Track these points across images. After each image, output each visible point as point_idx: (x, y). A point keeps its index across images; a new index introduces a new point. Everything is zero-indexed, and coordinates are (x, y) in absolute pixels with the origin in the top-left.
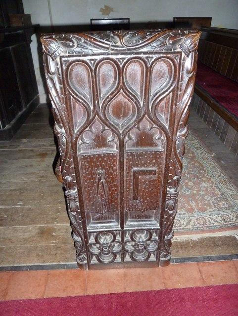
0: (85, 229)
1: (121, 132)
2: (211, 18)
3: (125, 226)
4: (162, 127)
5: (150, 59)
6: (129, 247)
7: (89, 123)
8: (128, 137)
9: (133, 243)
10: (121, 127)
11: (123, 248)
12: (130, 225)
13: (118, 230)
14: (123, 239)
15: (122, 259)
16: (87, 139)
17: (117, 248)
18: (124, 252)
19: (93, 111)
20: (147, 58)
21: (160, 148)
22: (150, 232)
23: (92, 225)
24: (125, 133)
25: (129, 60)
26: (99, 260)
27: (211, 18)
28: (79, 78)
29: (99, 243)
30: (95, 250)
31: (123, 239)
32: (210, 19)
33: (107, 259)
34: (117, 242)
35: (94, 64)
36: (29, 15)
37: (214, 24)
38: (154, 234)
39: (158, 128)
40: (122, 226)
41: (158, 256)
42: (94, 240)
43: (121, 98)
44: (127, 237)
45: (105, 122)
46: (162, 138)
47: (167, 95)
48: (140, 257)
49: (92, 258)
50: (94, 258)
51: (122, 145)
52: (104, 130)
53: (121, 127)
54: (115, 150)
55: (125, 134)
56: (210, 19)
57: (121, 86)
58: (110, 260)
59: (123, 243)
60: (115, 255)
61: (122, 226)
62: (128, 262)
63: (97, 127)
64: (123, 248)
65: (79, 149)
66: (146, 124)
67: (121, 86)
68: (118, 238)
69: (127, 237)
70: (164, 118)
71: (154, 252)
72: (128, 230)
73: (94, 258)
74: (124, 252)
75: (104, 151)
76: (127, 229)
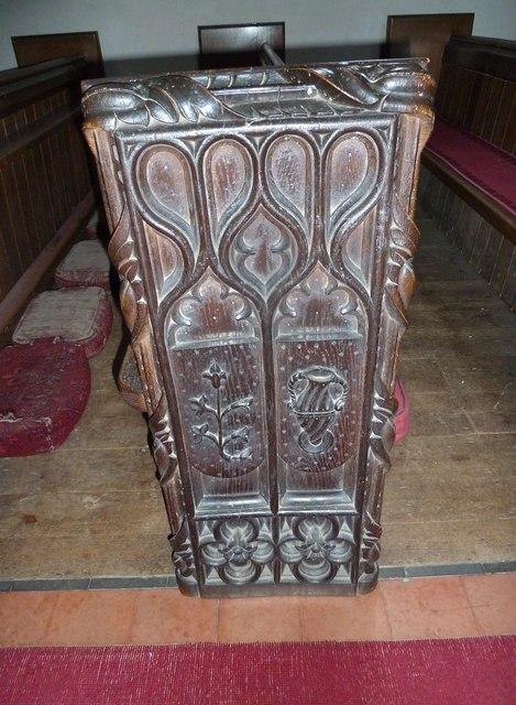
0: (189, 509)
1: (266, 299)
2: (473, 15)
3: (280, 507)
4: (355, 288)
5: (322, 136)
6: (291, 552)
7: (188, 282)
8: (281, 310)
9: (300, 543)
10: (164, 287)
11: (277, 552)
12: (289, 501)
13: (264, 516)
14: (276, 536)
15: (352, 579)
16: (186, 311)
17: (263, 554)
18: (277, 563)
19: (200, 259)
20: (313, 132)
21: (354, 331)
22: (333, 522)
23: (205, 504)
24: (275, 300)
25: (279, 135)
26: (297, 575)
27: (473, 15)
28: (163, 177)
29: (303, 539)
30: (215, 557)
31: (276, 536)
32: (468, 19)
33: (240, 575)
34: (263, 541)
35: (261, 145)
36: (95, 33)
37: (480, 30)
38: (265, 526)
39: (347, 290)
40: (274, 507)
41: (355, 577)
42: (291, 532)
43: (260, 220)
44: (286, 530)
45: (230, 281)
46: (253, 315)
47: (365, 214)
48: (240, 575)
49: (201, 530)
50: (214, 573)
51: (267, 330)
52: (227, 294)
53: (265, 289)
54: (253, 336)
55: (275, 300)
56: (468, 19)
57: (260, 203)
58: (325, 575)
59: (276, 546)
60: (258, 568)
61: (274, 507)
62: (288, 584)
63: (209, 286)
64: (277, 552)
65: (172, 342)
66: (321, 282)
67: (260, 203)
68: (265, 531)
69: (286, 530)
70: (356, 265)
71: (346, 565)
72: (284, 515)
73: (214, 573)
74: (277, 563)
75: (229, 338)
76: (283, 512)
